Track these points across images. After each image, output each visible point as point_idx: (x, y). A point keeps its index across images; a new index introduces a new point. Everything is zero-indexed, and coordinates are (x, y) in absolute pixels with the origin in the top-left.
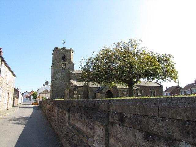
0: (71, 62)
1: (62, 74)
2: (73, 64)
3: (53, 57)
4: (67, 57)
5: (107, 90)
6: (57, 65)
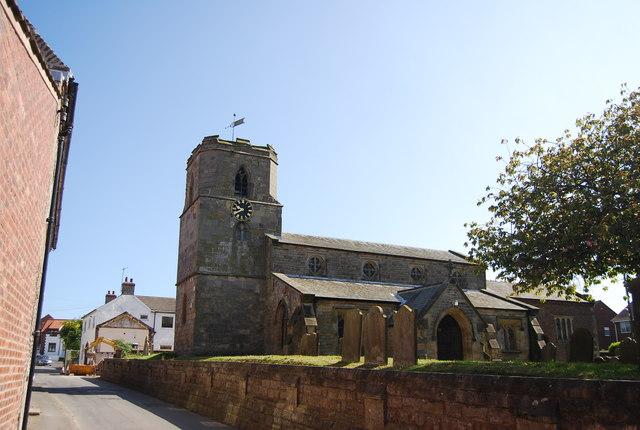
0: (270, 199)
1: (234, 249)
2: (279, 209)
3: (190, 177)
4: (256, 180)
5: (443, 315)
6: (217, 207)
